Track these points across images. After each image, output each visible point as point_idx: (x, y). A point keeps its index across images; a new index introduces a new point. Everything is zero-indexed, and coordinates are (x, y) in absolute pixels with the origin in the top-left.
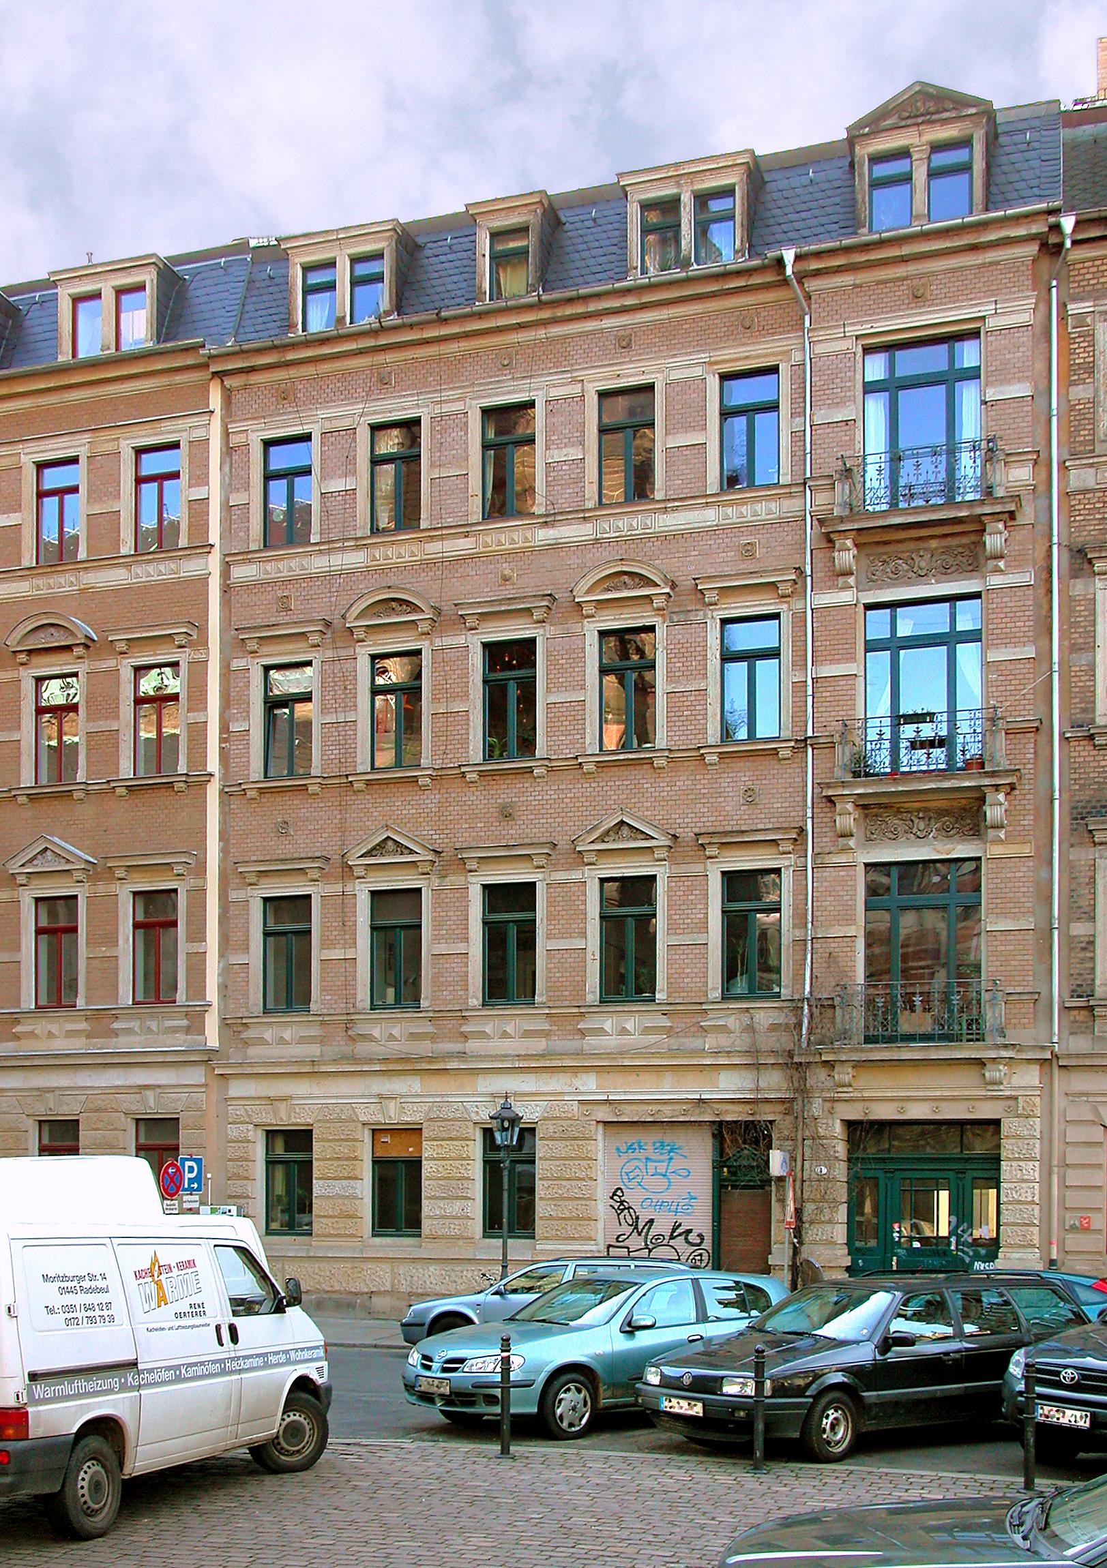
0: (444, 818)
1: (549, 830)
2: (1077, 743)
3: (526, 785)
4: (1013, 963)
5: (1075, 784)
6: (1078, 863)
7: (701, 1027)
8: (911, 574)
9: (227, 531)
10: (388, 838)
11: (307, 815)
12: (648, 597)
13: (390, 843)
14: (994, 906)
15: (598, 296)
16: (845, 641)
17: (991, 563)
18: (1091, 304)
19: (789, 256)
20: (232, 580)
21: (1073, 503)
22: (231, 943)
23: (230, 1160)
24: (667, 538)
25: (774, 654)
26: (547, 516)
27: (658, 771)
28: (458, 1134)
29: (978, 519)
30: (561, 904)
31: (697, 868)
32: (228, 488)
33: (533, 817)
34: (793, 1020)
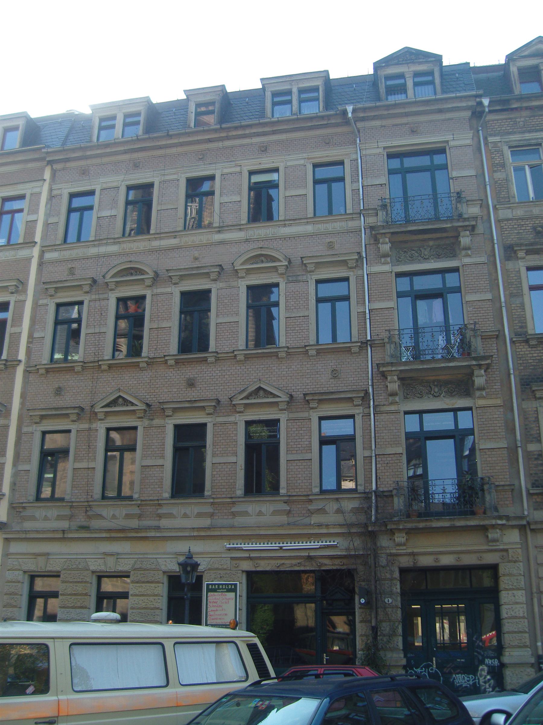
0: (154, 386)
1: (216, 393)
2: (519, 344)
3: (203, 368)
4: (497, 468)
5: (521, 366)
6: (527, 410)
7: (309, 510)
8: (420, 258)
9: (44, 236)
10: (120, 397)
11: (73, 384)
12: (275, 267)
14: (482, 434)
15: (250, 126)
16: (386, 291)
17: (464, 252)
18: (499, 138)
19: (350, 109)
20: (45, 259)
21: (502, 225)
22: (21, 458)
23: (6, 594)
24: (285, 238)
25: (346, 298)
26: (219, 227)
27: (280, 360)
28: (153, 579)
29: (456, 229)
30: (222, 436)
31: (305, 415)
32: (48, 215)
33: (206, 386)
34: (365, 506)
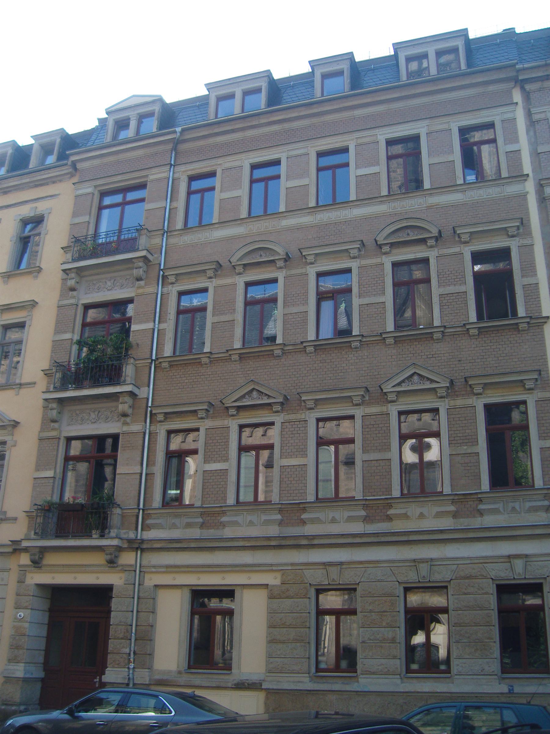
13: (416, 378)
